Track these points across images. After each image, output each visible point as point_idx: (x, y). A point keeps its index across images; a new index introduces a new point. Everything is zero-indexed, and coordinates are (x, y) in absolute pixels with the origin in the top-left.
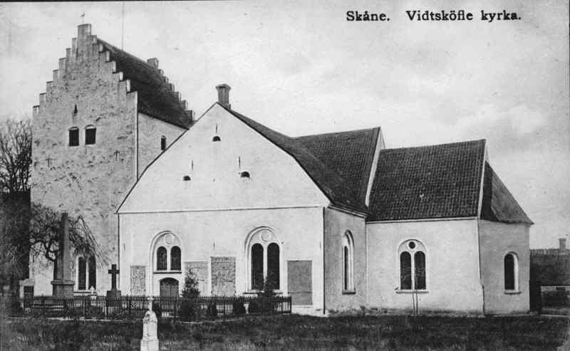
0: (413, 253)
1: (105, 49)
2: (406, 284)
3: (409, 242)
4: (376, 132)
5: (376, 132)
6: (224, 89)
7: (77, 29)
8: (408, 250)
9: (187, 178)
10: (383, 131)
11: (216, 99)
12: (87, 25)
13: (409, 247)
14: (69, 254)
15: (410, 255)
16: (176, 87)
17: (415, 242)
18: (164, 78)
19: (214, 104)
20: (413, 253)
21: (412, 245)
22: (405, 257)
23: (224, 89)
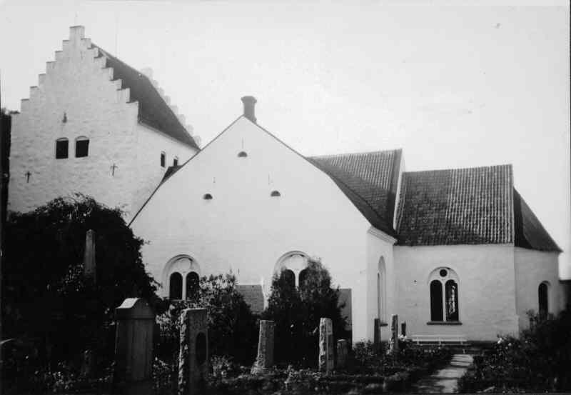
0: (443, 281)
1: (100, 55)
2: (436, 316)
3: (439, 270)
4: (396, 156)
5: (396, 156)
6: (249, 103)
7: (89, 154)
8: (440, 279)
9: (208, 197)
10: (403, 150)
11: (242, 112)
12: (80, 27)
13: (444, 278)
14: (394, 347)
15: (441, 284)
16: (187, 120)
17: (448, 271)
18: (140, 254)
19: (240, 118)
20: (443, 281)
21: (443, 273)
22: (435, 286)
23: (249, 103)
